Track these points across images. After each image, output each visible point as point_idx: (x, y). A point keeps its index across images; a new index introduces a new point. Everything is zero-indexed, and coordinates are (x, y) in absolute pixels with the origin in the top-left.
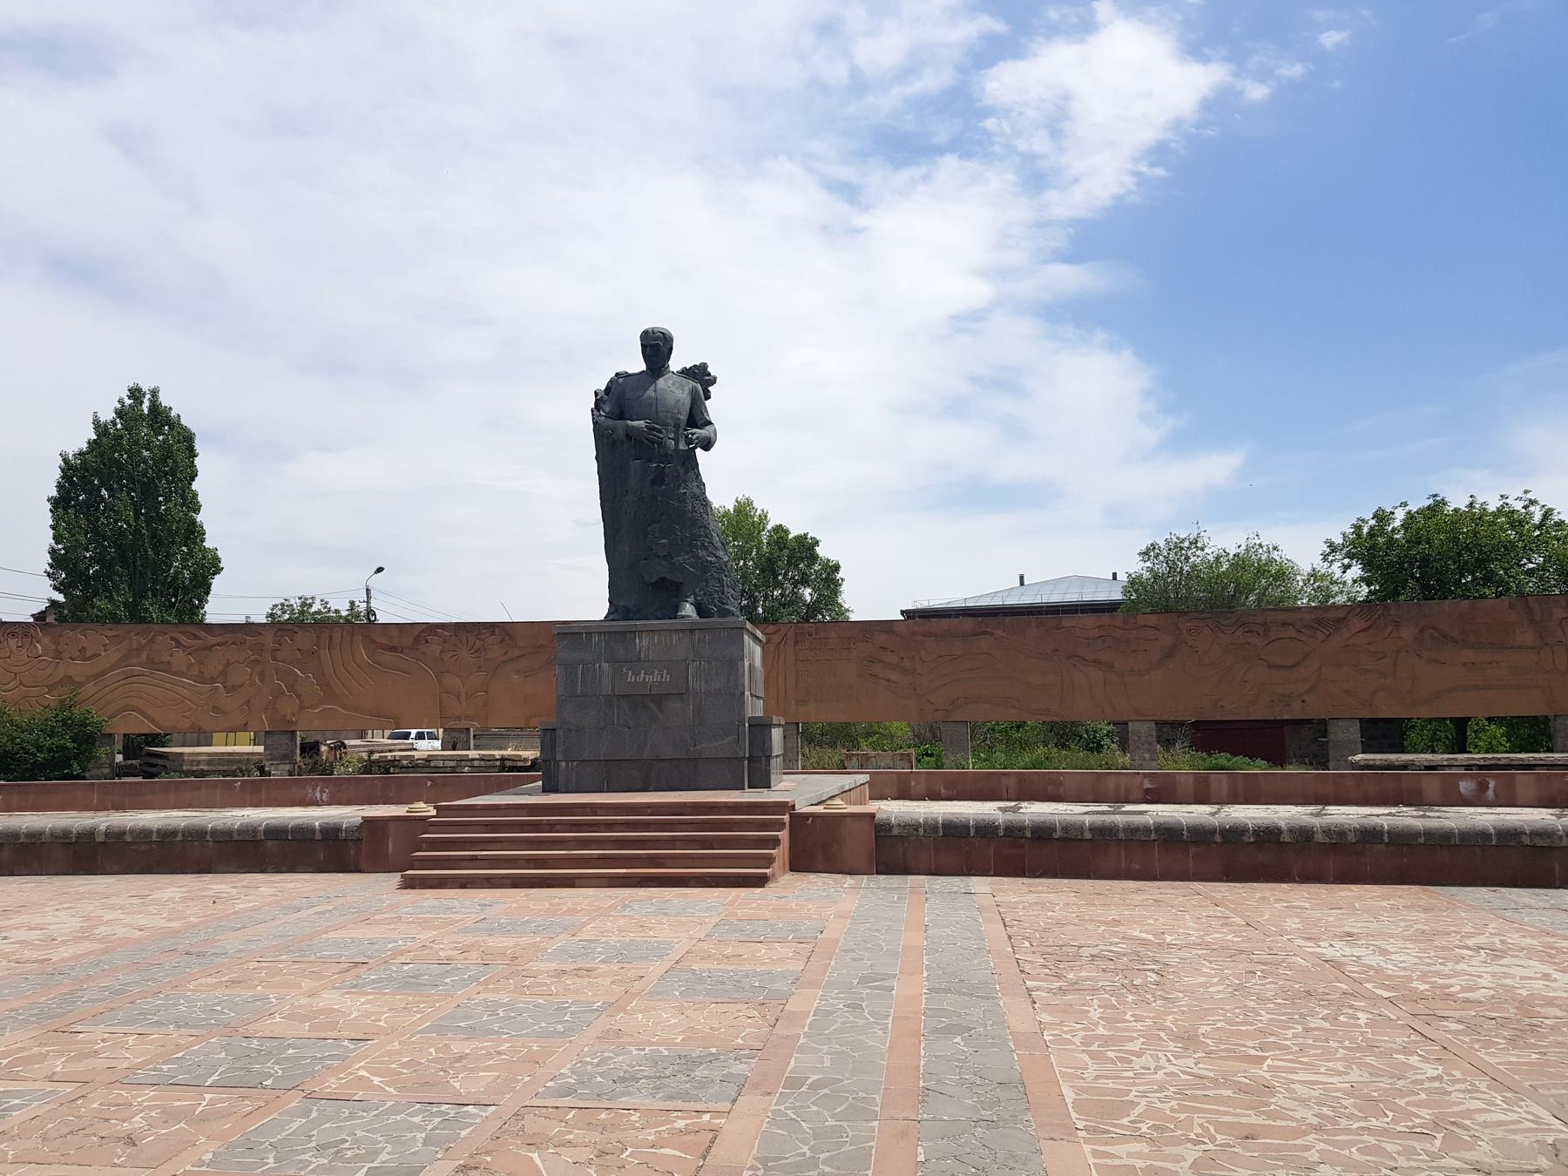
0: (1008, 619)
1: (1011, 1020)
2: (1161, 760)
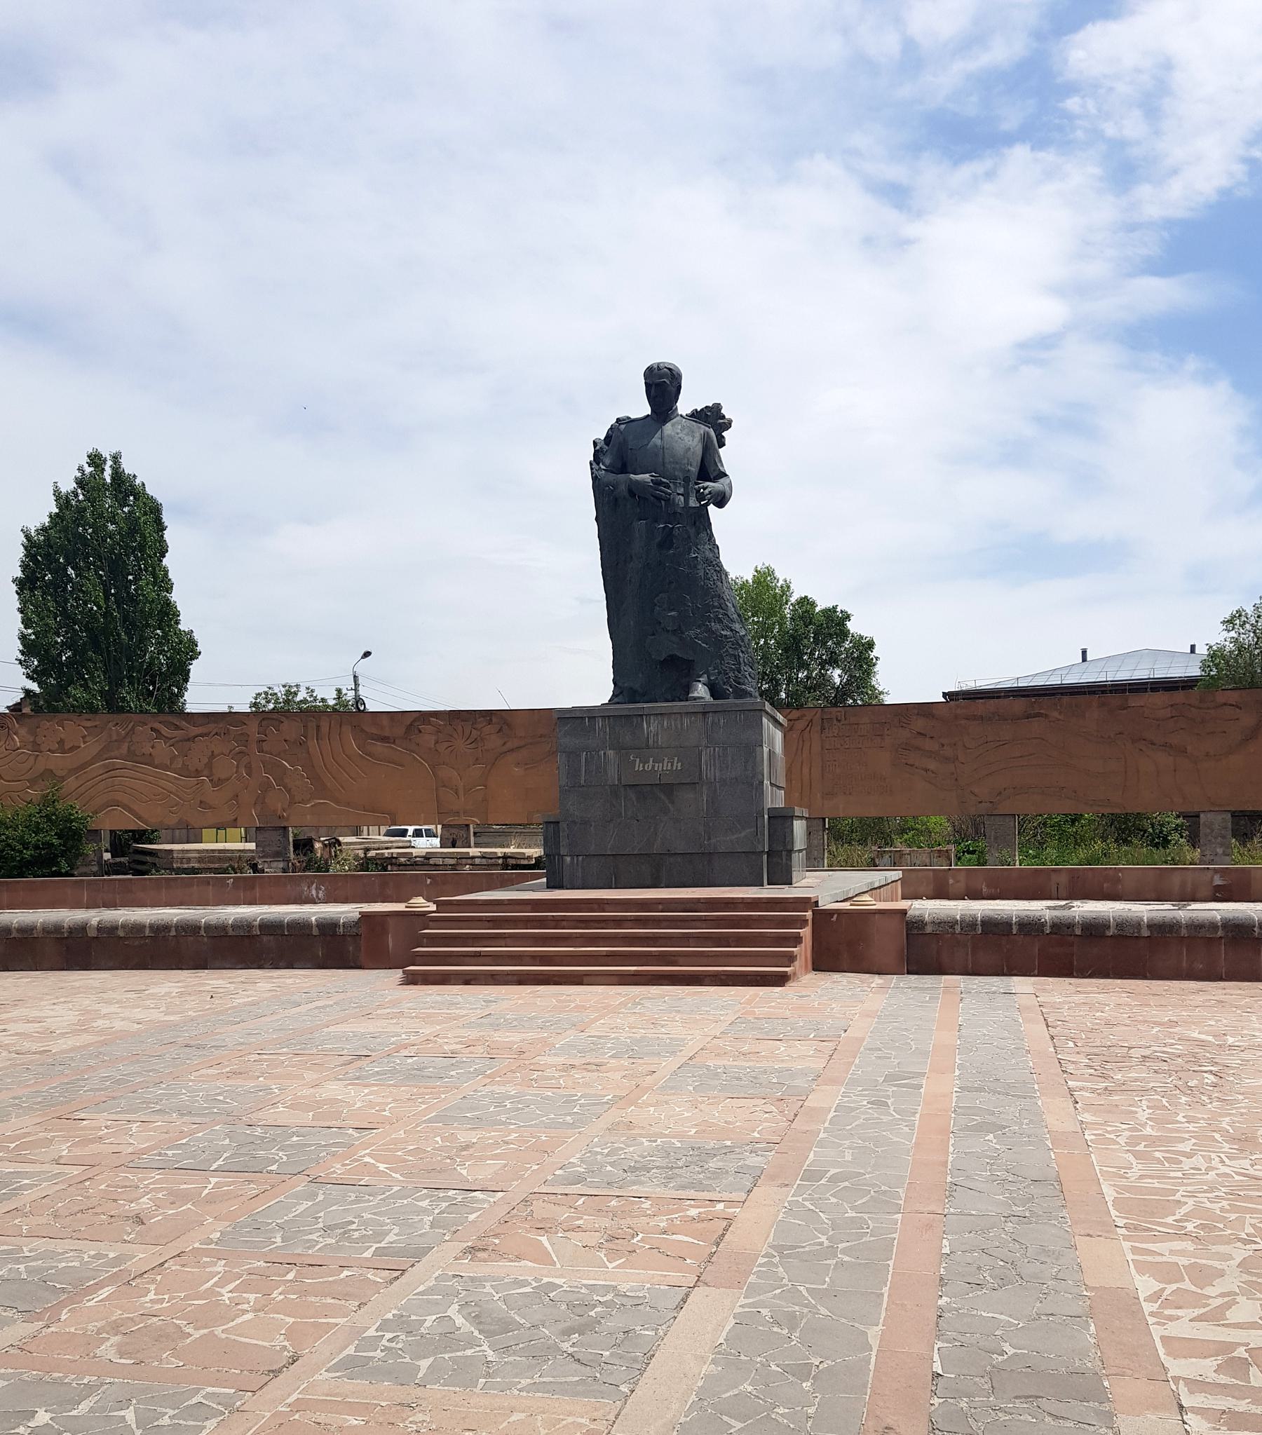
0: (1066, 699)
1: (1050, 1120)
2: (1236, 856)
